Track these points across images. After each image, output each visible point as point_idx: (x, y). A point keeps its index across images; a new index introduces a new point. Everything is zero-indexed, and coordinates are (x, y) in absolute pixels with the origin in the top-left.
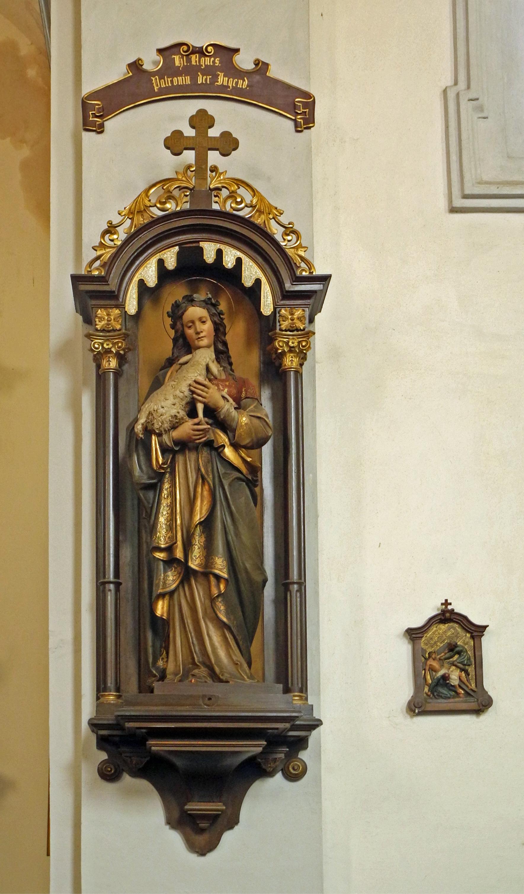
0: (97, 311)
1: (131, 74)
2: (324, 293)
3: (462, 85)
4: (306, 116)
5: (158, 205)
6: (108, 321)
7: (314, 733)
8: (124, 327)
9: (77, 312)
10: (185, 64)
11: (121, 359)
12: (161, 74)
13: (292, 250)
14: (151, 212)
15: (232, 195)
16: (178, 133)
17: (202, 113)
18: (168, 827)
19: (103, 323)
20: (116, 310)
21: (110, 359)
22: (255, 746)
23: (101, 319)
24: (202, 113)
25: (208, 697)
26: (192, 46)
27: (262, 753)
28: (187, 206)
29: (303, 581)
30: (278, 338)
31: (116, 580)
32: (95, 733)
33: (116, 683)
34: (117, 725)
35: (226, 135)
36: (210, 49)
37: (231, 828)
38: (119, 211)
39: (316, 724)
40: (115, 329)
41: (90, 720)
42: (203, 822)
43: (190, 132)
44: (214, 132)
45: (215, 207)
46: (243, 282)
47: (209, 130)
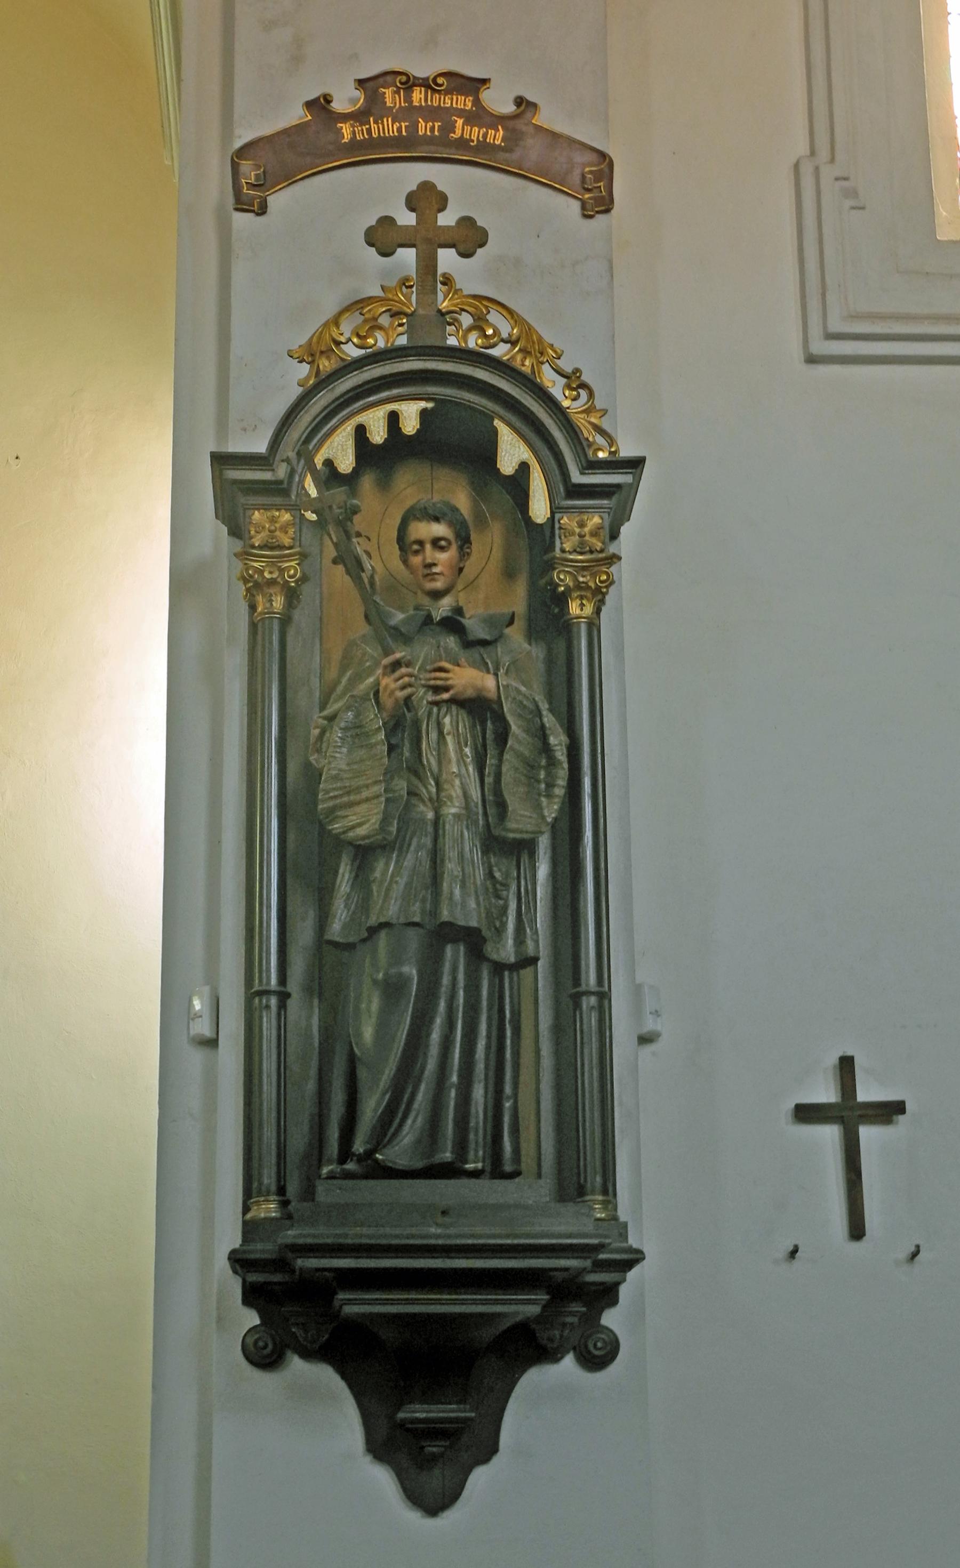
0: (253, 514)
1: (310, 118)
2: (633, 491)
3: (824, 154)
4: (601, 192)
5: (355, 340)
6: (270, 531)
7: (632, 1275)
8: (298, 544)
9: (217, 517)
10: (403, 104)
11: (292, 596)
12: (359, 117)
13: (582, 416)
14: (343, 352)
15: (479, 325)
16: (387, 221)
17: (427, 187)
18: (369, 1458)
19: (262, 534)
20: (287, 513)
21: (273, 598)
22: (529, 1302)
23: (260, 528)
24: (427, 187)
25: (440, 1210)
26: (413, 76)
27: (539, 1316)
28: (403, 341)
29: (607, 989)
30: (556, 566)
31: (282, 989)
32: (239, 1275)
33: (279, 1181)
34: (280, 1264)
35: (467, 222)
36: (440, 80)
37: (486, 1460)
38: (289, 351)
39: (633, 1259)
40: (281, 544)
41: (233, 1252)
42: (434, 1443)
43: (407, 219)
44: (446, 219)
45: (452, 341)
46: (498, 466)
47: (439, 215)
